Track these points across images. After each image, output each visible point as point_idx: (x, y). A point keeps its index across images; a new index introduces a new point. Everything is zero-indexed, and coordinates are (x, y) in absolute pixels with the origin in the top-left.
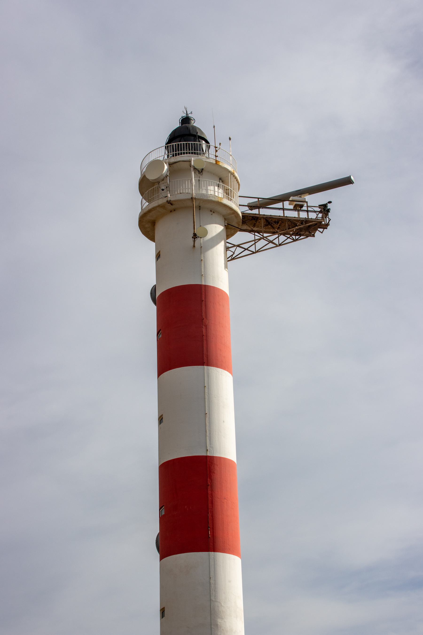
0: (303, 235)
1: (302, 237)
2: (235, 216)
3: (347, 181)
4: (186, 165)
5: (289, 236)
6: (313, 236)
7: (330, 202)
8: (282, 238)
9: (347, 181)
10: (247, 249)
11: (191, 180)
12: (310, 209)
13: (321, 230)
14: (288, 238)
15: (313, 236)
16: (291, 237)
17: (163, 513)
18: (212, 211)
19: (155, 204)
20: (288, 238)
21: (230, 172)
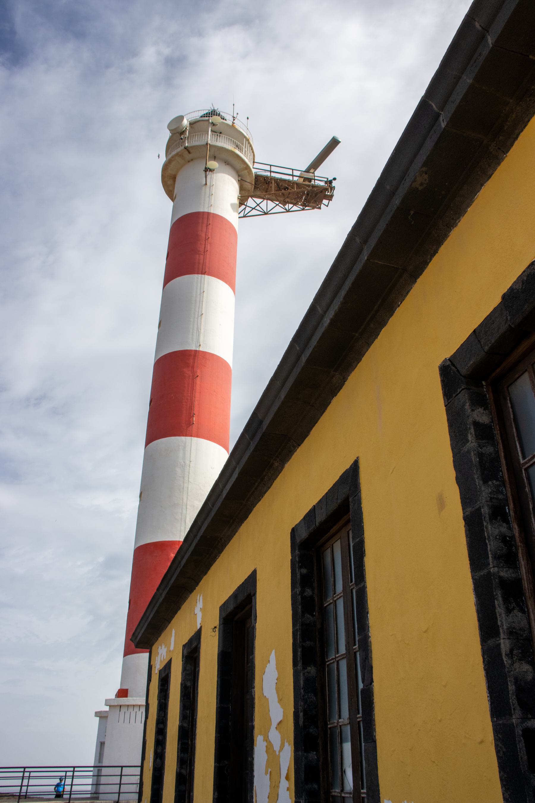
0: (308, 206)
1: (307, 208)
2: (248, 172)
3: (334, 143)
4: (206, 123)
5: (277, 203)
6: (320, 208)
7: (335, 179)
8: (271, 204)
9: (334, 143)
10: (253, 209)
11: (208, 135)
12: (316, 178)
13: (325, 202)
14: (277, 205)
15: (320, 208)
16: (258, 208)
17: (216, 797)
18: (227, 163)
19: (304, 183)
20: (277, 205)
21: (245, 137)
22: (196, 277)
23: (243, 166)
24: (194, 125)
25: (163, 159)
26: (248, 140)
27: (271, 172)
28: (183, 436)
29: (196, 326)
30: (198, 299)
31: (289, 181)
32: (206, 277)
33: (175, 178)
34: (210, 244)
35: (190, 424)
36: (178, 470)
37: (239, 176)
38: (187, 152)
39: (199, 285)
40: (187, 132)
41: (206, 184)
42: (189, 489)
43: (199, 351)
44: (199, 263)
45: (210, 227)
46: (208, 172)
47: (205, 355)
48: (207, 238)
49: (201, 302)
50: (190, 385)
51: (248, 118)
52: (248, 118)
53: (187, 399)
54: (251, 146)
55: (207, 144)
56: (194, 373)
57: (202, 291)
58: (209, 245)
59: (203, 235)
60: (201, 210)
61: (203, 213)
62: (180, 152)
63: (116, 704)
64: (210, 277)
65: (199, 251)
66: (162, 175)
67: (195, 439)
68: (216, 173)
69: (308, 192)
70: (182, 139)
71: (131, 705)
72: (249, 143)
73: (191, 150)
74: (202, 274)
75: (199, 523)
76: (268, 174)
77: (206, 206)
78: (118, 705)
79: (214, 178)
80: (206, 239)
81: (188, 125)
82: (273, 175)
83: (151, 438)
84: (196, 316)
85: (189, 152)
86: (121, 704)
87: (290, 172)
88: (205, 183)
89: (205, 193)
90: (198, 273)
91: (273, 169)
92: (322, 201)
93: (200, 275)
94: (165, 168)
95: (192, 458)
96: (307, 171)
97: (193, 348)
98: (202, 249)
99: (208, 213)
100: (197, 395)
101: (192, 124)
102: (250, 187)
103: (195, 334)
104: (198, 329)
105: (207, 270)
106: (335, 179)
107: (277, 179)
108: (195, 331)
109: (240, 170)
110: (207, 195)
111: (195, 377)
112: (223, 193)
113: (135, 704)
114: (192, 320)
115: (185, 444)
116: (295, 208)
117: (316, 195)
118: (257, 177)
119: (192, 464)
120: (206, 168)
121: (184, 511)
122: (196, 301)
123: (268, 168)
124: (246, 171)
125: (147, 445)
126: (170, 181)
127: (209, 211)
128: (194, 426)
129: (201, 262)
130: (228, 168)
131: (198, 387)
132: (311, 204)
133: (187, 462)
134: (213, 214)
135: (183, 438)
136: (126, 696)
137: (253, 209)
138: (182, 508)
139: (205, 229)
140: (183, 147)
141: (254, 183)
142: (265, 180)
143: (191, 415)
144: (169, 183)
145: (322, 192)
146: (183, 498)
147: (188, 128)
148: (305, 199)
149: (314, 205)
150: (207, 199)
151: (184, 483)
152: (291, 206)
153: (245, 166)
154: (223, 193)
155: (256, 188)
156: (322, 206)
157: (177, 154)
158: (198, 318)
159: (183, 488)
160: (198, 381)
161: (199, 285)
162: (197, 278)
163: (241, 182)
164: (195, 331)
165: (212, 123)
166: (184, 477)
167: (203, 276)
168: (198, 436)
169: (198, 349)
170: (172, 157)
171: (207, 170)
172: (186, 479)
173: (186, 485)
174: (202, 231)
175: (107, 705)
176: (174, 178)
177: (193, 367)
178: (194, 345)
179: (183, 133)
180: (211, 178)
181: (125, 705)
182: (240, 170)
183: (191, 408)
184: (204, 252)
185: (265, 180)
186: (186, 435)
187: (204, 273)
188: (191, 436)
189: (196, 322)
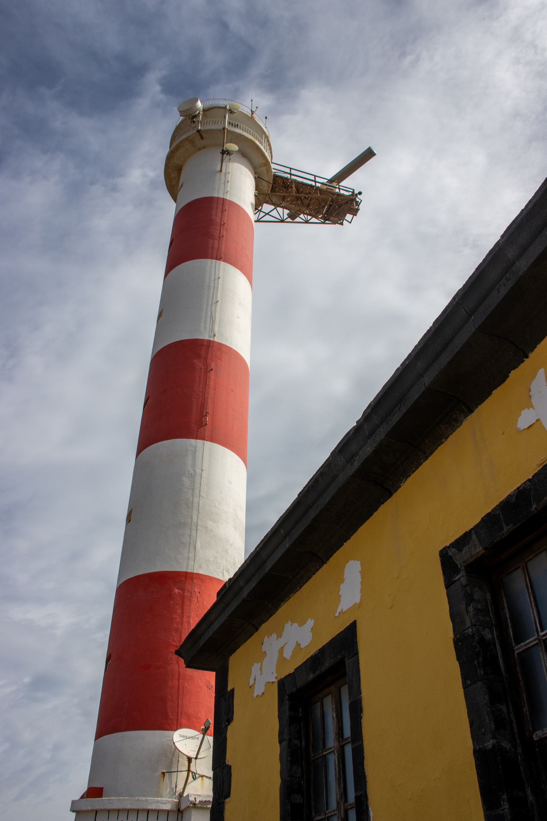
1: (327, 222)
6: (342, 224)
7: (360, 193)
10: (268, 214)
12: (341, 187)
13: (349, 217)
15: (342, 224)
21: (264, 133)
22: (209, 263)
23: (262, 161)
24: (207, 113)
25: (168, 150)
26: (267, 137)
27: (291, 174)
28: (193, 438)
29: (209, 314)
30: (212, 285)
31: (311, 186)
32: (222, 263)
33: (181, 169)
34: (227, 230)
35: (201, 424)
36: (186, 481)
37: (255, 173)
38: (199, 137)
39: (213, 270)
40: (201, 116)
41: (221, 171)
42: (200, 504)
43: (213, 342)
44: (213, 248)
45: (226, 213)
46: (225, 155)
47: (221, 346)
48: (222, 223)
49: (216, 288)
50: (202, 379)
51: (266, 118)
52: (266, 118)
53: (199, 395)
54: (270, 145)
55: (224, 128)
56: (207, 365)
57: (217, 277)
58: (224, 231)
59: (218, 220)
60: (216, 195)
61: (218, 198)
62: (190, 136)
63: (90, 808)
64: (226, 264)
65: (213, 236)
66: (166, 165)
67: (208, 444)
68: (233, 162)
69: (332, 201)
70: (194, 122)
71: (114, 810)
72: (268, 141)
73: (204, 135)
74: (216, 259)
75: (511, 253)
76: (289, 176)
77: (222, 192)
78: (92, 811)
79: (230, 166)
80: (221, 225)
81: (202, 110)
82: (293, 177)
83: (147, 439)
84: (210, 303)
85: (202, 138)
86: (97, 808)
87: (312, 178)
88: (219, 169)
89: (220, 179)
90: (212, 258)
91: (293, 172)
92: (345, 216)
93: (214, 260)
94: (169, 158)
95: (205, 467)
96: (331, 181)
97: (206, 338)
98: (216, 234)
99: (223, 199)
100: (211, 391)
101: (205, 110)
102: (266, 188)
103: (208, 322)
104: (211, 316)
105: (223, 256)
106: (360, 193)
107: (299, 183)
108: (209, 319)
109: (259, 165)
110: (222, 182)
111: (208, 370)
112: (241, 186)
113: (120, 807)
114: (205, 307)
115: (196, 448)
116: (314, 220)
117: (339, 207)
118: (276, 177)
119: (204, 474)
120: (223, 150)
121: (194, 533)
122: (209, 287)
123: (288, 170)
124: (264, 168)
125: (139, 452)
126: (173, 176)
127: (225, 198)
128: (207, 427)
129: (216, 246)
130: (244, 160)
131: (212, 383)
132: (331, 218)
133: (198, 471)
134: (230, 201)
135: (193, 441)
136: (101, 796)
137: (268, 214)
138: (191, 529)
139: (219, 214)
140: (195, 131)
141: (271, 182)
142: (284, 182)
143: (202, 415)
144: (173, 175)
145: (347, 203)
146: (192, 517)
147: (201, 113)
148: (327, 211)
149: (336, 219)
150: (222, 186)
151: (193, 496)
152: (309, 217)
153: (264, 162)
154: (241, 186)
155: (273, 190)
156: (345, 222)
157: (187, 139)
158: (212, 305)
159: (192, 504)
160: (212, 375)
161: (213, 270)
162: (212, 263)
163: (258, 179)
164: (209, 319)
165: (230, 110)
166: (193, 490)
167: (218, 261)
168: (212, 440)
169: (212, 339)
170: (181, 142)
171: (223, 152)
172: (197, 491)
173: (196, 499)
174: (216, 216)
175: (73, 811)
176: (179, 170)
177: (206, 359)
178: (207, 334)
179: (195, 116)
180: (227, 165)
181: (105, 810)
182: (259, 165)
183: (203, 405)
184: (219, 238)
185: (284, 182)
186: (197, 438)
187: (218, 258)
188: (203, 439)
189: (209, 309)
